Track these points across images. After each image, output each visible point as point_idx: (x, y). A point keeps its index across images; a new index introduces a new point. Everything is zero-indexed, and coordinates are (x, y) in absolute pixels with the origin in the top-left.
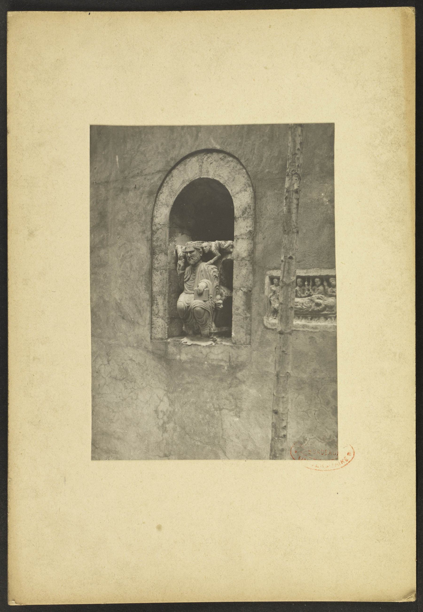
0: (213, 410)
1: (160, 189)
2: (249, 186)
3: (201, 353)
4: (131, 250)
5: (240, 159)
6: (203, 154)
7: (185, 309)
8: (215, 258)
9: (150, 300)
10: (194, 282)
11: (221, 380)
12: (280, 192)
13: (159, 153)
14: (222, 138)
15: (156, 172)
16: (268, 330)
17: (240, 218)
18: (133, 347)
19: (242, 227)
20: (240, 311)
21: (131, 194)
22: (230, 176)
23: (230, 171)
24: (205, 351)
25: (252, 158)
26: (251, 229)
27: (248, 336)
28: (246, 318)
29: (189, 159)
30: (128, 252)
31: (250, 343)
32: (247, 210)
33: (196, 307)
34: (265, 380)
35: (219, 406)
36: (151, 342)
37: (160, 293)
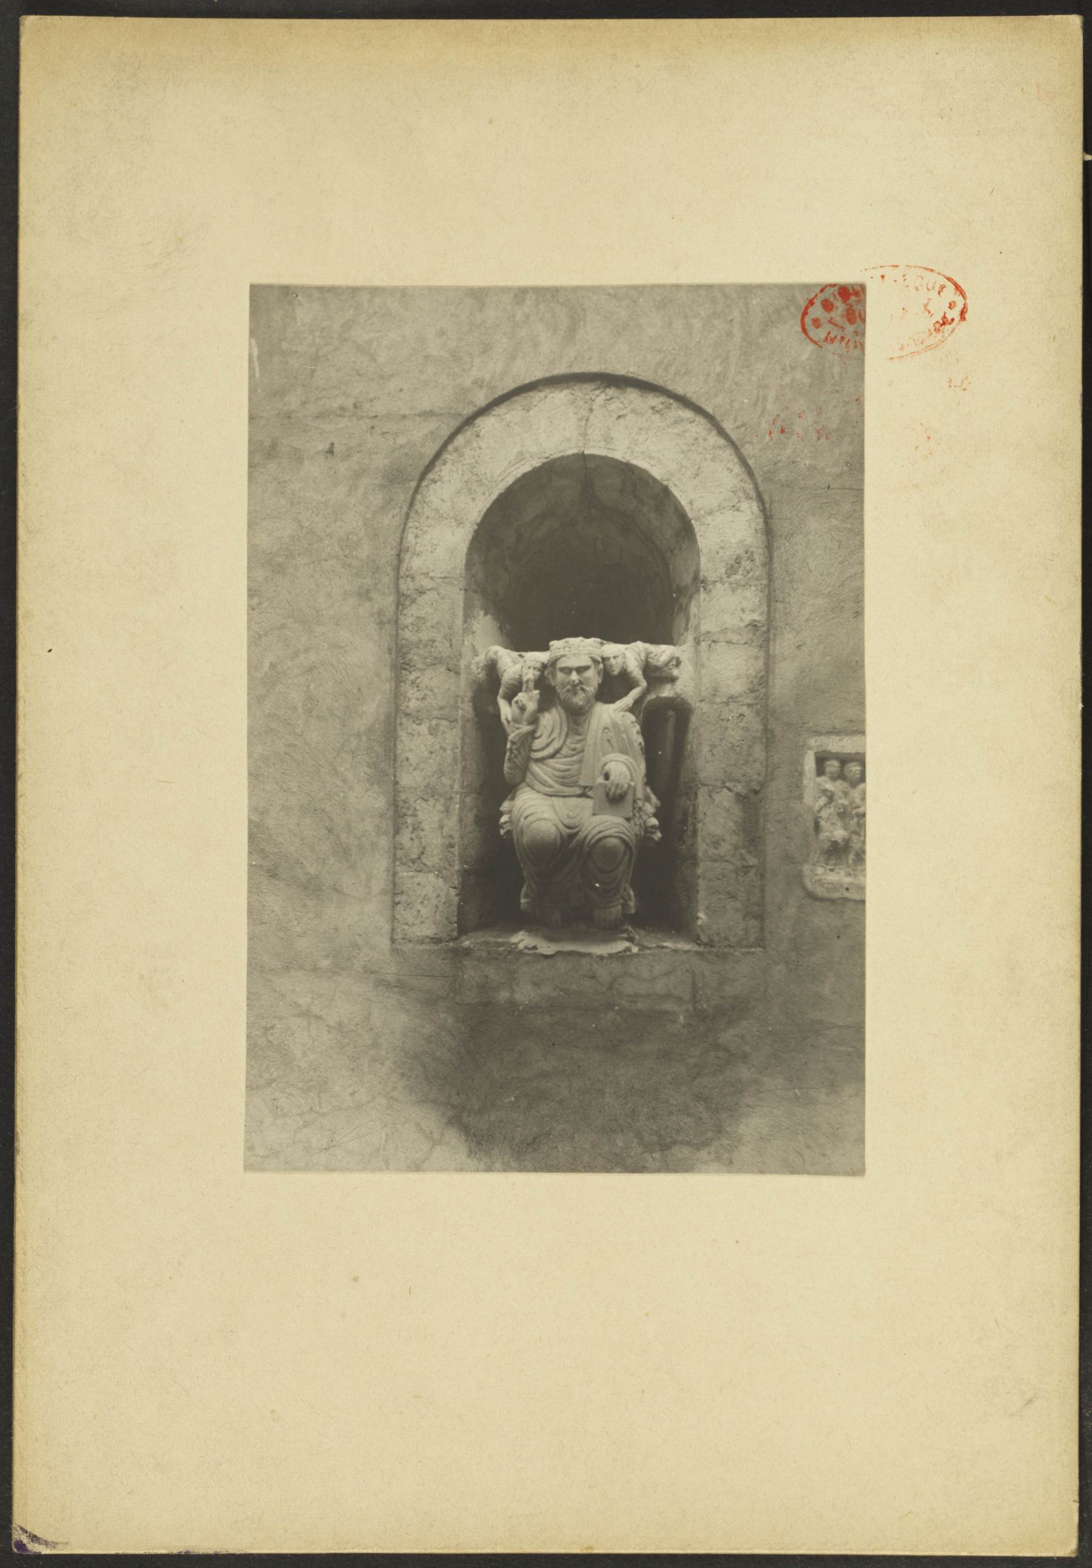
0: (639, 1150)
1: (429, 467)
2: (748, 497)
3: (593, 977)
4: (307, 650)
5: (718, 418)
6: (593, 386)
7: (559, 841)
8: (635, 693)
9: (390, 814)
10: (581, 761)
11: (665, 1056)
12: (849, 526)
13: (427, 357)
14: (660, 351)
15: (420, 415)
16: (817, 903)
17: (718, 585)
18: (315, 969)
19: (723, 607)
20: (725, 848)
21: (313, 468)
22: (685, 463)
23: (685, 448)
24: (603, 974)
25: (760, 423)
26: (756, 616)
27: (754, 923)
28: (746, 869)
29: (542, 394)
30: (296, 654)
31: (761, 942)
32: (743, 563)
33: (605, 837)
34: (812, 1046)
35: (660, 1136)
36: (393, 950)
37: (430, 792)
